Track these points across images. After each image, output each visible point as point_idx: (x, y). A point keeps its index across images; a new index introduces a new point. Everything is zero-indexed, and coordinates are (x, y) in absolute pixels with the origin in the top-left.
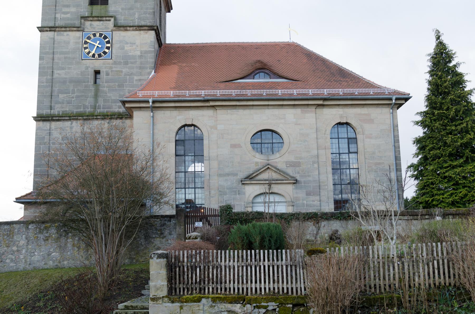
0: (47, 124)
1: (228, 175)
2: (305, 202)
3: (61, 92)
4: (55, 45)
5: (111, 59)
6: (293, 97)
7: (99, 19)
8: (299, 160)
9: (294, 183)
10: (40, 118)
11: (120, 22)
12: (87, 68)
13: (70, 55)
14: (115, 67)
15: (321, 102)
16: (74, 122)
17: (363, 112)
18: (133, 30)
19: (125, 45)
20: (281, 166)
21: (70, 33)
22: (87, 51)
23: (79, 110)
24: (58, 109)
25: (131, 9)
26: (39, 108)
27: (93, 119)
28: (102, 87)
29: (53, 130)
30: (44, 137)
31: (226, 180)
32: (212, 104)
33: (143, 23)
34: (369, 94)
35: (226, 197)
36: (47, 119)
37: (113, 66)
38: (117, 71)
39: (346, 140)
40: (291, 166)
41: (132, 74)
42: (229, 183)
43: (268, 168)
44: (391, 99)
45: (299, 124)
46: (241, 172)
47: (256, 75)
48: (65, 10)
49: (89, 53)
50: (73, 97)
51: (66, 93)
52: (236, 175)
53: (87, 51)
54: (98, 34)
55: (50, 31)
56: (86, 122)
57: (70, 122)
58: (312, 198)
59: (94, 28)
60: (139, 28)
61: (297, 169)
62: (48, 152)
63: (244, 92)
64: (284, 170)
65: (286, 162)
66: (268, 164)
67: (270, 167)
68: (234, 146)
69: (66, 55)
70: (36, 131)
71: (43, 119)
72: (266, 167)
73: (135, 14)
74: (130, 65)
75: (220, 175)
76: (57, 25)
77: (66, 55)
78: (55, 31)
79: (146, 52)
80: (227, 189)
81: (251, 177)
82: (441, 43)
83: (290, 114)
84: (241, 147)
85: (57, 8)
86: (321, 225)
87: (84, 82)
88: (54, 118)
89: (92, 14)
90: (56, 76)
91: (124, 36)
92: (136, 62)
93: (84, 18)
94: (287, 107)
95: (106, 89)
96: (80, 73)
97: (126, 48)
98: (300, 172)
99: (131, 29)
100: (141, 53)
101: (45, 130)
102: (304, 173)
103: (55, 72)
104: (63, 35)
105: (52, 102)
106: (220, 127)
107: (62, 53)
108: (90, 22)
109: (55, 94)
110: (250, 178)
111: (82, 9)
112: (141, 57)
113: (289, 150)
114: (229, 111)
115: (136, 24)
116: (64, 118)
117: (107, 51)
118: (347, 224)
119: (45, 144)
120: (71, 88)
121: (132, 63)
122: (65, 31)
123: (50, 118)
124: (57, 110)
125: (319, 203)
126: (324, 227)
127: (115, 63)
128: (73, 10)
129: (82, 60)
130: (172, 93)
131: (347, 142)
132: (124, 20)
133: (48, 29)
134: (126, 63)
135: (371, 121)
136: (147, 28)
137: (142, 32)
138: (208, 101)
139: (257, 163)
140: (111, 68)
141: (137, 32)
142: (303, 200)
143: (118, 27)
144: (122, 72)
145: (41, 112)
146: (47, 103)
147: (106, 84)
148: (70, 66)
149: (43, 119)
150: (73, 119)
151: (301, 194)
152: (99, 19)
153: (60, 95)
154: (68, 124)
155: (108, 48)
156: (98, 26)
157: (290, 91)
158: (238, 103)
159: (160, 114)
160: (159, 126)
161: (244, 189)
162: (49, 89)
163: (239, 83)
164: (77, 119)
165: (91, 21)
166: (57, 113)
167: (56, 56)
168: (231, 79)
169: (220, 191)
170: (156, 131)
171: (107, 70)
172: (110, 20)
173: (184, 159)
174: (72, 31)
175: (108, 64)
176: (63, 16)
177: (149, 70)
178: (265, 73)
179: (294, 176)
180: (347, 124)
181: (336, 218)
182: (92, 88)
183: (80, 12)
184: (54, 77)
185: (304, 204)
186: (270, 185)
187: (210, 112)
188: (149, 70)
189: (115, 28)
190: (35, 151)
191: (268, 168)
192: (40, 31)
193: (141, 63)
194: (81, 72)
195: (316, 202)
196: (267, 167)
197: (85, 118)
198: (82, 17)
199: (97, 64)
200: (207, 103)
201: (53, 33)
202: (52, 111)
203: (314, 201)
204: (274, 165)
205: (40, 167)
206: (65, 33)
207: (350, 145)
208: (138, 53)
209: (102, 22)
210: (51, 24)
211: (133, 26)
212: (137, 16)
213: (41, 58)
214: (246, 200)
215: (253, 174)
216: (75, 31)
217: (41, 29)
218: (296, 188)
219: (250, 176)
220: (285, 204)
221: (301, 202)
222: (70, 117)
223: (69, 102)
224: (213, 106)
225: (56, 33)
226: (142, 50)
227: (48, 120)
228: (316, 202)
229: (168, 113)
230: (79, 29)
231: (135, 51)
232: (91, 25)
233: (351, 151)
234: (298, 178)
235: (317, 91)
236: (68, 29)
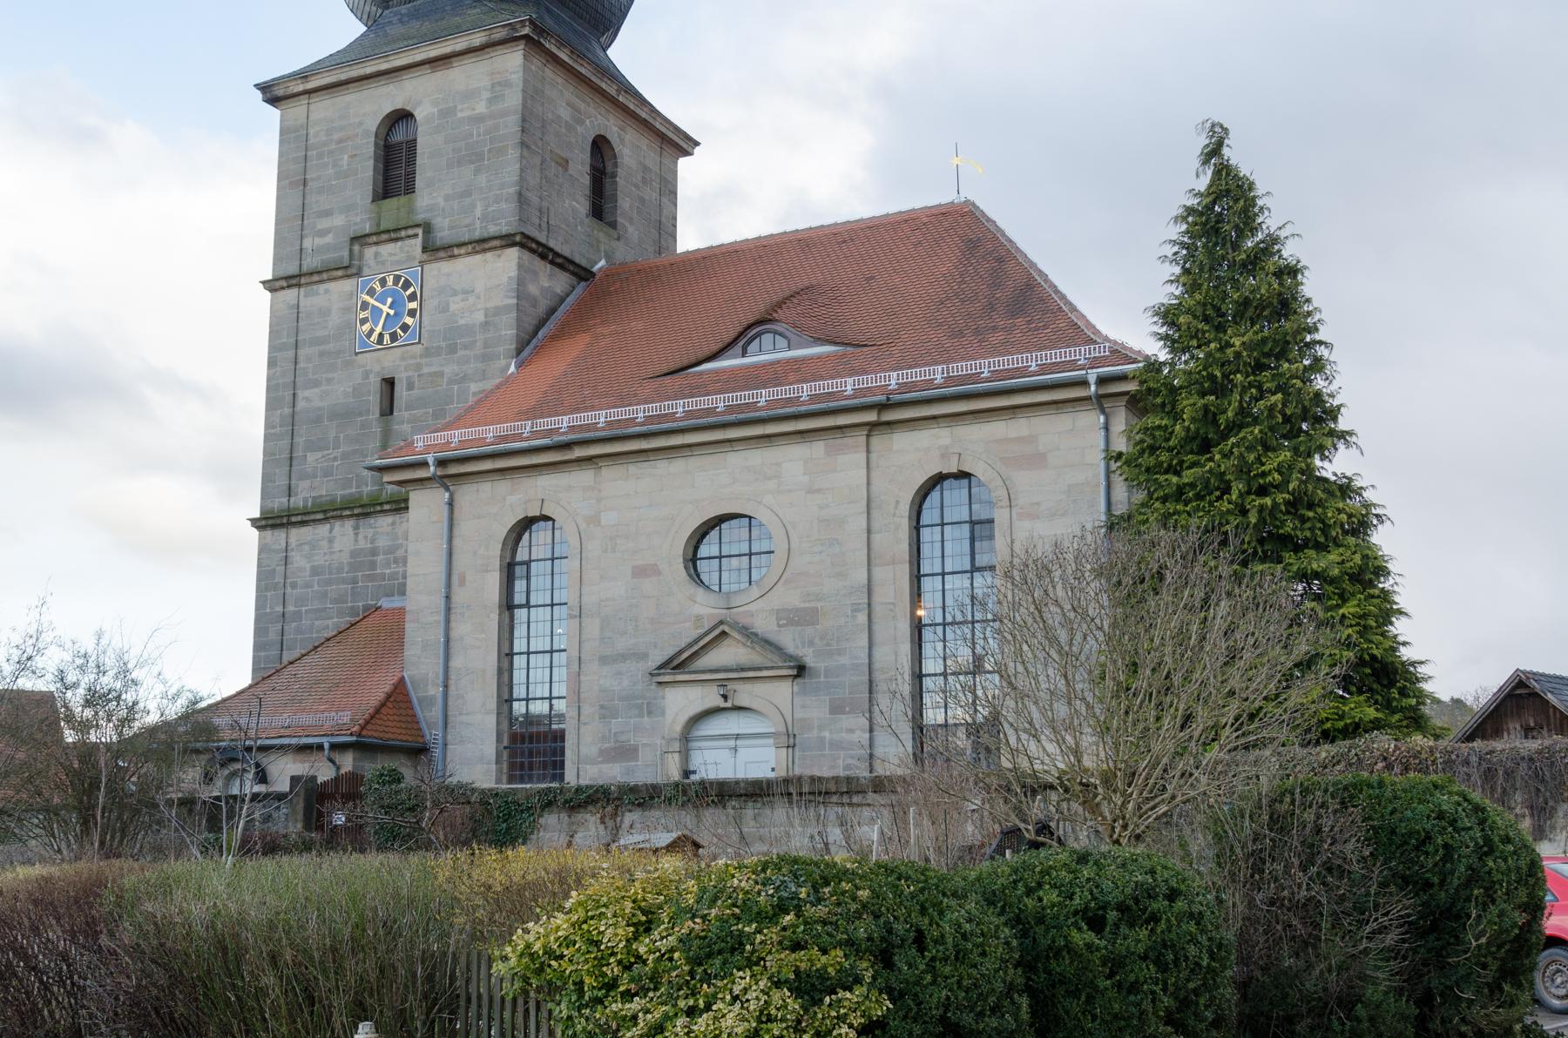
0: (280, 534)
1: (623, 657)
2: (827, 734)
3: (311, 447)
6: (557, 439)
7: (393, 235)
10: (268, 522)
12: (366, 374)
13: (330, 347)
15: (871, 417)
16: (338, 524)
17: (1013, 434)
18: (468, 254)
20: (764, 624)
21: (332, 285)
22: (366, 327)
24: (305, 494)
32: (579, 452)
33: (493, 230)
34: (671, 417)
37: (423, 361)
38: (430, 374)
39: (966, 527)
40: (791, 622)
42: (626, 683)
43: (724, 633)
44: (1084, 383)
45: (819, 491)
48: (323, 224)
49: (372, 331)
50: (335, 459)
51: (321, 449)
52: (643, 656)
53: (366, 327)
55: (289, 287)
56: (361, 522)
58: (847, 721)
59: (383, 263)
60: (481, 244)
61: (809, 630)
62: (279, 609)
63: (743, 397)
64: (772, 637)
65: (778, 611)
66: (721, 623)
67: (727, 629)
68: (640, 572)
72: (717, 632)
74: (461, 353)
75: (604, 660)
78: (299, 285)
79: (498, 311)
81: (676, 662)
82: (1224, 172)
83: (793, 462)
87: (360, 414)
88: (294, 519)
89: (378, 225)
90: (301, 405)
91: (449, 275)
93: (359, 239)
94: (782, 441)
95: (406, 427)
97: (453, 307)
98: (817, 641)
99: (462, 251)
101: (277, 551)
103: (301, 394)
106: (608, 518)
108: (374, 249)
109: (298, 453)
110: (678, 665)
114: (633, 469)
115: (477, 235)
116: (312, 517)
117: (409, 320)
120: (332, 435)
121: (465, 347)
122: (321, 282)
127: (428, 353)
128: (338, 221)
130: (490, 432)
132: (451, 228)
133: (284, 284)
135: (1037, 460)
137: (489, 255)
139: (699, 618)
140: (418, 367)
141: (478, 257)
142: (821, 728)
143: (435, 250)
144: (441, 374)
145: (270, 505)
147: (406, 414)
151: (814, 710)
152: (393, 235)
154: (323, 529)
155: (412, 313)
156: (391, 254)
157: (961, 368)
160: (464, 528)
162: (286, 442)
163: (701, 373)
164: (341, 517)
165: (376, 243)
167: (301, 352)
170: (457, 542)
172: (416, 235)
174: (335, 279)
176: (319, 241)
177: (503, 362)
178: (776, 333)
182: (377, 429)
184: (298, 408)
185: (822, 740)
188: (503, 362)
189: (425, 256)
192: (272, 290)
193: (486, 346)
195: (858, 733)
196: (719, 635)
198: (354, 239)
200: (566, 453)
201: (295, 290)
203: (851, 731)
206: (322, 287)
207: (977, 544)
208: (480, 317)
212: (478, 212)
213: (272, 363)
215: (680, 652)
217: (271, 286)
220: (771, 741)
221: (815, 733)
222: (324, 512)
227: (281, 525)
229: (486, 488)
232: (376, 255)
234: (809, 661)
235: (654, 408)
236: (325, 276)
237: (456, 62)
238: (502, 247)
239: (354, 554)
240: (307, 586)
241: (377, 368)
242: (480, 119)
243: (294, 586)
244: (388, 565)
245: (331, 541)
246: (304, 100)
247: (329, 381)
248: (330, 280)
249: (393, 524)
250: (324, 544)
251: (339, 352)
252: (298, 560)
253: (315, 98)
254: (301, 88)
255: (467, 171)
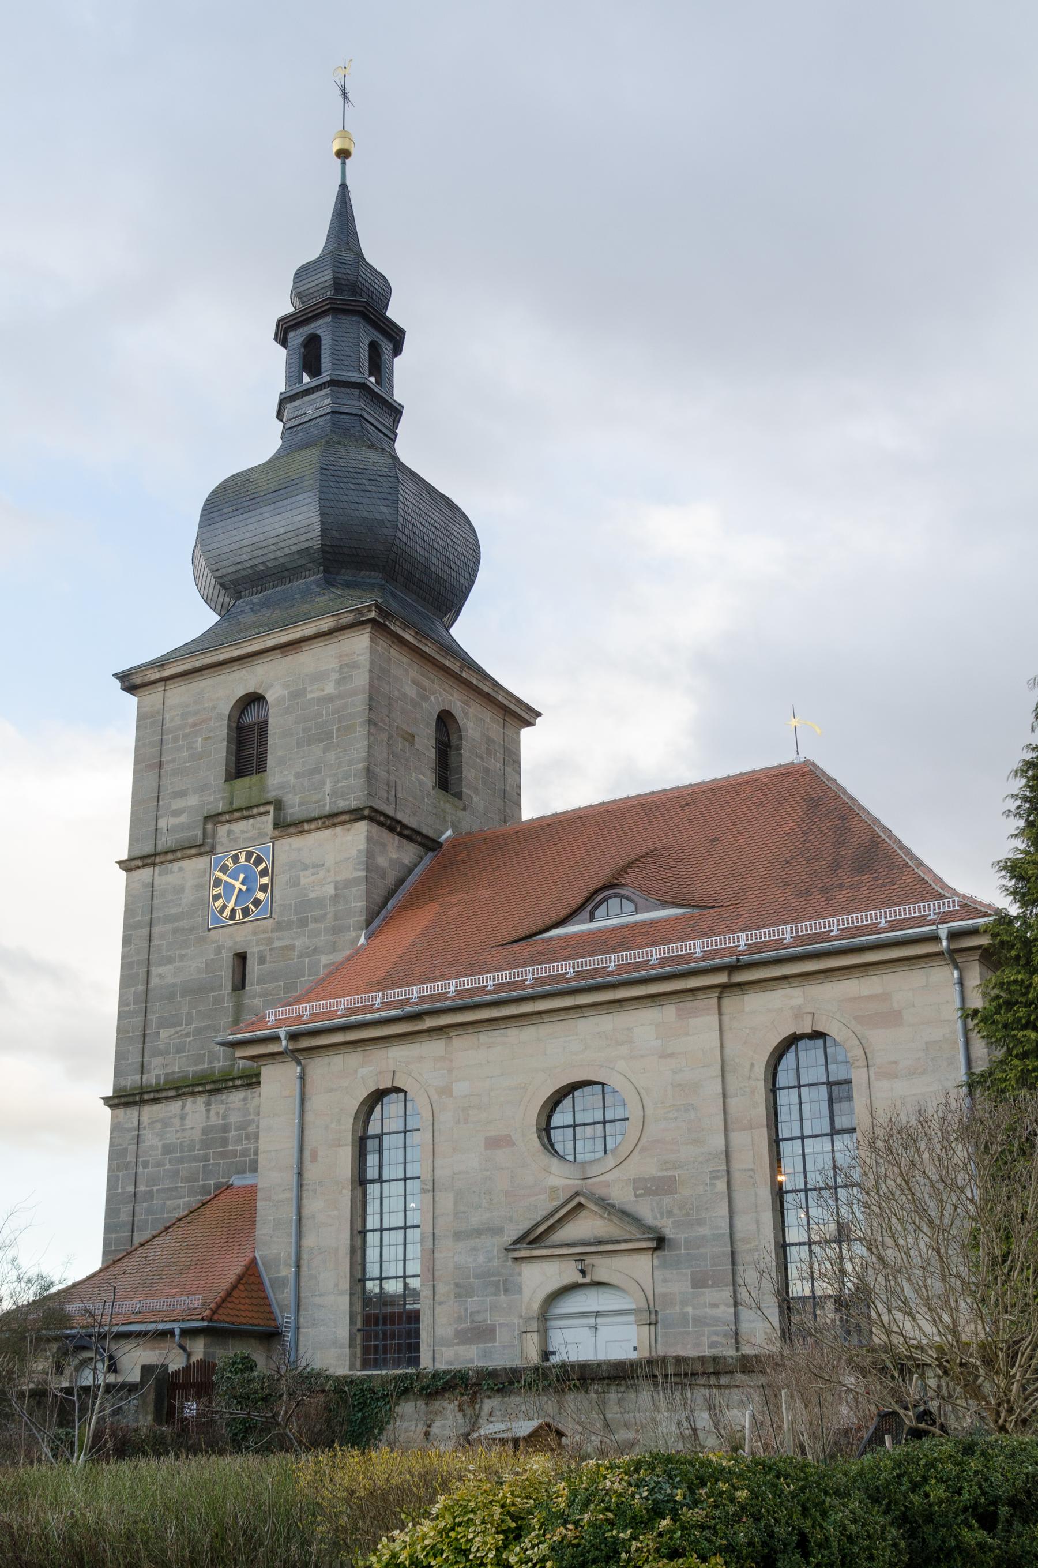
0: (133, 1113)
1: (478, 1232)
2: (689, 1310)
3: (164, 1024)
4: (155, 901)
5: (271, 917)
7: (245, 813)
8: (670, 1173)
9: (655, 1249)
11: (290, 811)
12: (219, 950)
13: (184, 923)
14: (279, 939)
16: (189, 1100)
17: (866, 992)
18: (318, 829)
19: (302, 874)
20: (621, 1195)
21: (185, 864)
22: (219, 903)
23: (200, 1067)
25: (316, 770)
26: (118, 1073)
27: (227, 1088)
28: (249, 998)
29: (144, 1128)
30: (126, 1149)
31: (474, 1249)
32: (430, 1023)
33: (342, 805)
35: (472, 1303)
36: (131, 1099)
37: (275, 935)
38: (282, 948)
39: (824, 1089)
40: (649, 1192)
41: (316, 950)
43: (580, 1205)
45: (671, 1055)
46: (511, 1221)
47: (597, 907)
48: (177, 804)
49: (224, 907)
50: (188, 1035)
52: (498, 1231)
53: (219, 903)
54: (244, 854)
55: (144, 866)
56: (213, 1098)
57: (180, 1103)
60: (331, 819)
61: (667, 1200)
62: (131, 1189)
64: (629, 1208)
67: (583, 1200)
68: (494, 1143)
69: (176, 924)
70: (111, 1133)
71: (123, 1100)
73: (324, 783)
74: (312, 926)
75: (458, 1236)
76: (160, 848)
77: (176, 924)
78: (154, 864)
79: (348, 884)
80: (476, 1276)
81: (532, 1237)
83: (645, 1025)
84: (514, 1144)
85: (161, 803)
86: (481, 1408)
87: (213, 990)
90: (154, 981)
91: (299, 850)
92: (326, 914)
93: (213, 818)
94: (635, 1005)
95: (258, 1002)
96: (203, 966)
97: (304, 881)
98: (676, 1211)
99: (313, 826)
100: (336, 889)
102: (688, 1214)
103: (155, 971)
104: (172, 872)
105: (146, 1054)
106: (460, 1088)
107: (168, 919)
108: (226, 827)
111: (210, 795)
112: (336, 898)
113: (643, 1140)
116: (164, 1094)
117: (261, 896)
118: (560, 1404)
119: (127, 1167)
121: (316, 920)
123: (137, 1098)
124: (157, 1072)
125: (732, 1310)
126: (491, 1414)
127: (279, 927)
128: (193, 800)
129: (209, 930)
130: (341, 1004)
131: (825, 1096)
132: (301, 804)
133: (139, 863)
134: (303, 922)
135: (893, 1018)
136: (346, 817)
137: (338, 830)
138: (418, 1016)
139: (554, 1190)
140: (270, 941)
141: (328, 832)
142: (684, 1303)
145: (123, 1083)
146: (135, 1059)
148: (183, 952)
149: (123, 1100)
150: (185, 1094)
151: (676, 1284)
152: (245, 813)
153: (162, 1031)
154: (175, 1107)
155: (264, 888)
156: (243, 832)
158: (494, 1013)
159: (320, 1069)
160: (317, 1102)
161: (520, 1274)
163: (550, 939)
165: (229, 821)
166: (154, 1081)
168: (527, 932)
169: (457, 1285)
170: (309, 1117)
171: (262, 948)
172: (267, 813)
173: (807, 1124)
174: (189, 857)
175: (265, 931)
176: (174, 821)
177: (353, 934)
178: (622, 897)
179: (658, 1223)
180: (817, 1035)
181: (499, 1391)
182: (229, 1004)
183: (209, 803)
184: (151, 985)
185: (684, 1316)
186: (580, 1258)
187: (434, 1047)
188: (353, 934)
189: (276, 833)
190: (108, 1190)
191: (580, 1205)
194: (207, 964)
195: (722, 1308)
197: (208, 1087)
199: (242, 937)
200: (417, 1024)
201: (149, 870)
202: (145, 1077)
203: (715, 1306)
204: (600, 1192)
205: (117, 1232)
206: (176, 866)
208: (330, 890)
209: (251, 821)
210: (148, 849)
211: (315, 819)
212: (328, 788)
214: (524, 1311)
216: (195, 855)
217: (126, 865)
218: (664, 1265)
219: (527, 1233)
220: (632, 1318)
221: (677, 1309)
222: (177, 1088)
223: (180, 1050)
224: (440, 1029)
225: (157, 869)
226: (338, 879)
227: (134, 1103)
228: (722, 1308)
229: (337, 1062)
230: (203, 850)
231: (322, 885)
232: (229, 832)
233: (838, 1126)
234: (669, 1232)
236: (179, 854)
237: (305, 647)
238: (352, 821)
239: (206, 1131)
240: (159, 1164)
241: (229, 943)
242: (330, 699)
243: (146, 1165)
244: (239, 1141)
245: (183, 1118)
246: (160, 687)
247: (182, 957)
248: (184, 858)
249: (245, 1099)
250: (176, 1121)
251: (192, 929)
252: (150, 1139)
253: (170, 685)
254: (157, 676)
255: (318, 749)
